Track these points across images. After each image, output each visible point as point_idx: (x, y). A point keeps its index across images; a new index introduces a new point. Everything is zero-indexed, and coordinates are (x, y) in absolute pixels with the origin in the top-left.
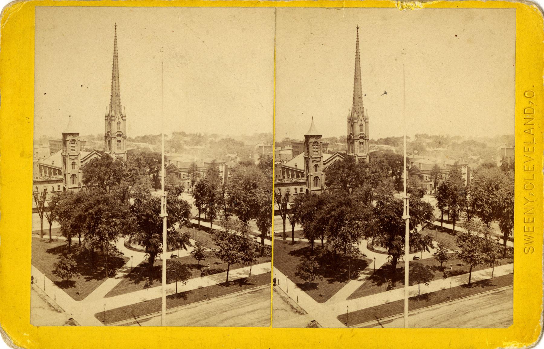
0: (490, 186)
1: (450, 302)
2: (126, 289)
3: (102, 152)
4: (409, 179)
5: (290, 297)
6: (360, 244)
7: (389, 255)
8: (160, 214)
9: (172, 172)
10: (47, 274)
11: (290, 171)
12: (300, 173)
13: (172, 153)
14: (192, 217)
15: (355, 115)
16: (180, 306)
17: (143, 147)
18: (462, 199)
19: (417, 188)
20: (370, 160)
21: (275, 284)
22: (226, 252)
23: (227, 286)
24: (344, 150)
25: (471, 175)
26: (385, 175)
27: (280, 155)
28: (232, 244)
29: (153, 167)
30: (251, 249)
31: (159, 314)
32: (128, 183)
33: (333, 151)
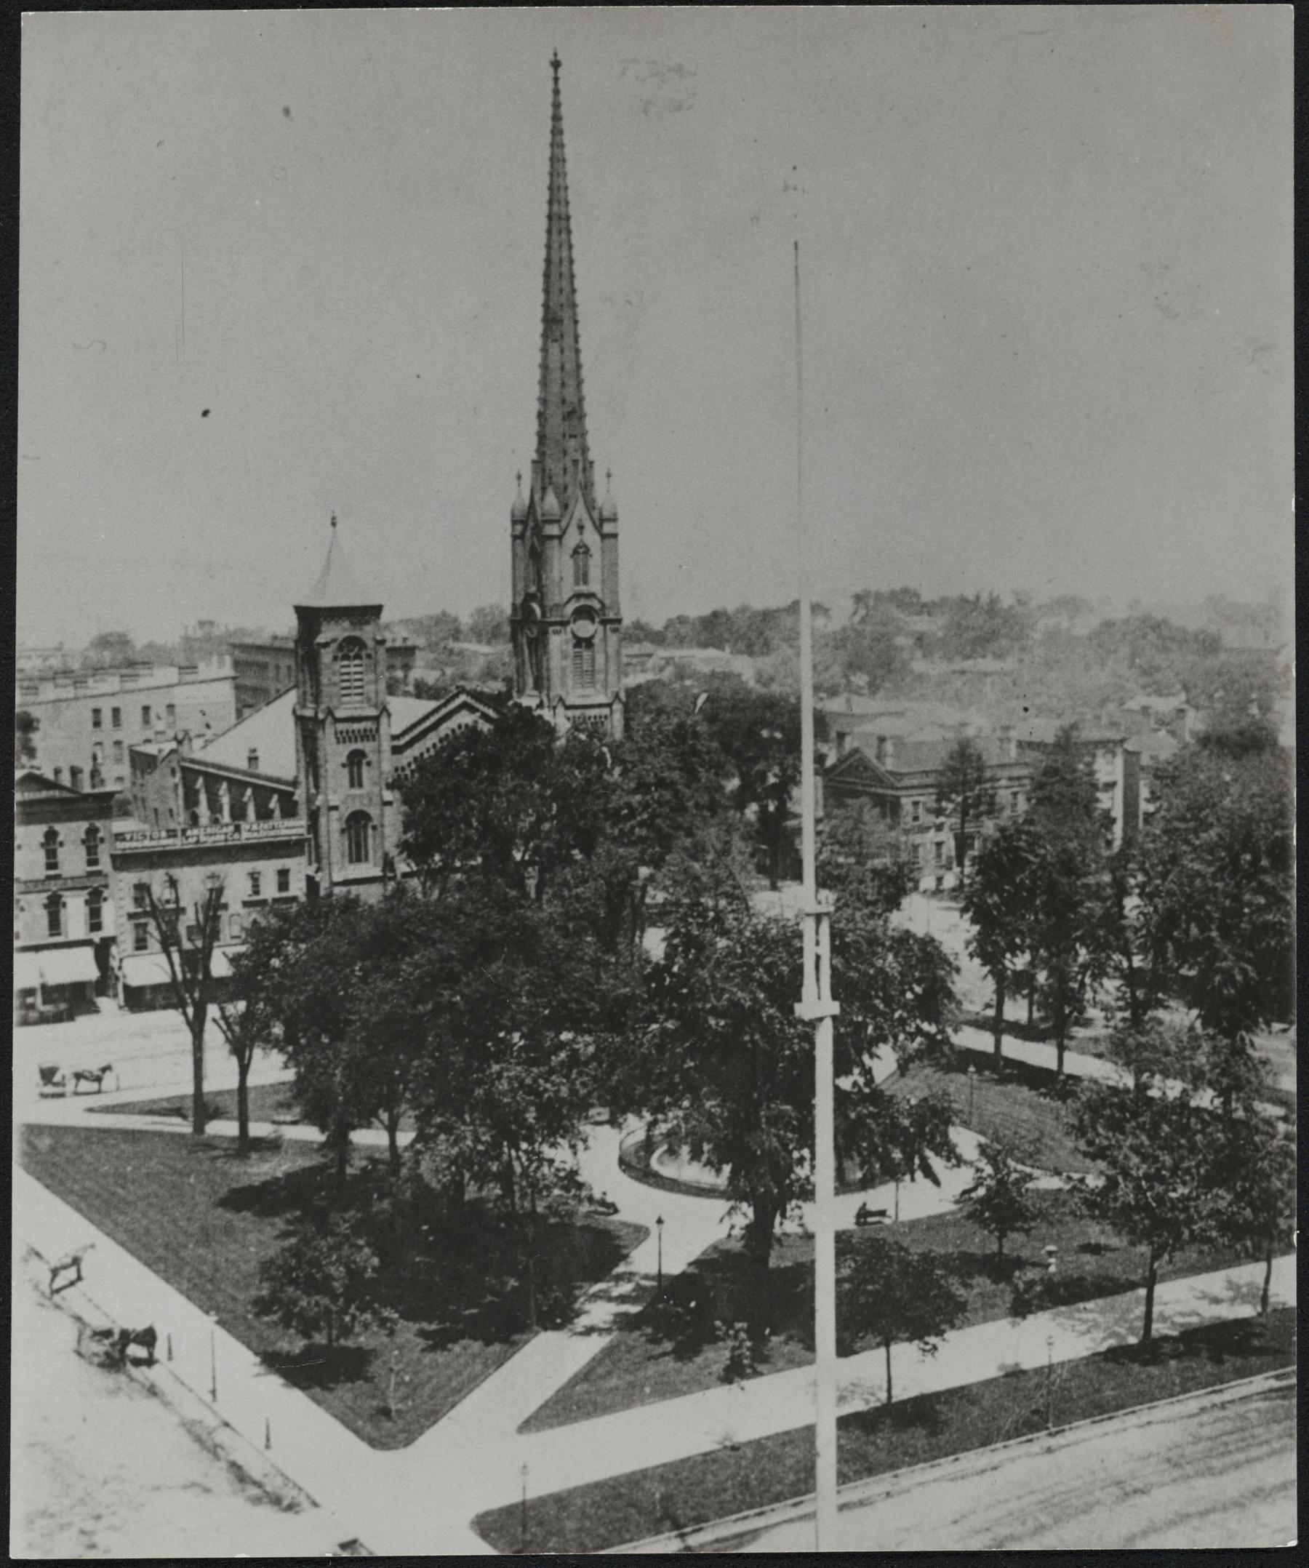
0: (1245, 850)
1: (1050, 1435)
2: (632, 1385)
3: (497, 701)
4: (828, 816)
5: (227, 1425)
6: (586, 1148)
7: (731, 1203)
8: (797, 1007)
9: (856, 794)
10: (225, 1316)
11: (224, 785)
12: (275, 797)
13: (855, 698)
14: (962, 1017)
15: (551, 502)
16: (910, 1465)
17: (706, 669)
18: (1099, 912)
19: (869, 864)
20: (627, 727)
21: (151, 1354)
22: (1138, 1189)
23: (1145, 1363)
24: (495, 678)
25: (1144, 792)
26: (704, 799)
27: (171, 707)
28: (1171, 1151)
29: (760, 766)
30: (1268, 1177)
31: (802, 1510)
32: (635, 852)
33: (440, 684)
